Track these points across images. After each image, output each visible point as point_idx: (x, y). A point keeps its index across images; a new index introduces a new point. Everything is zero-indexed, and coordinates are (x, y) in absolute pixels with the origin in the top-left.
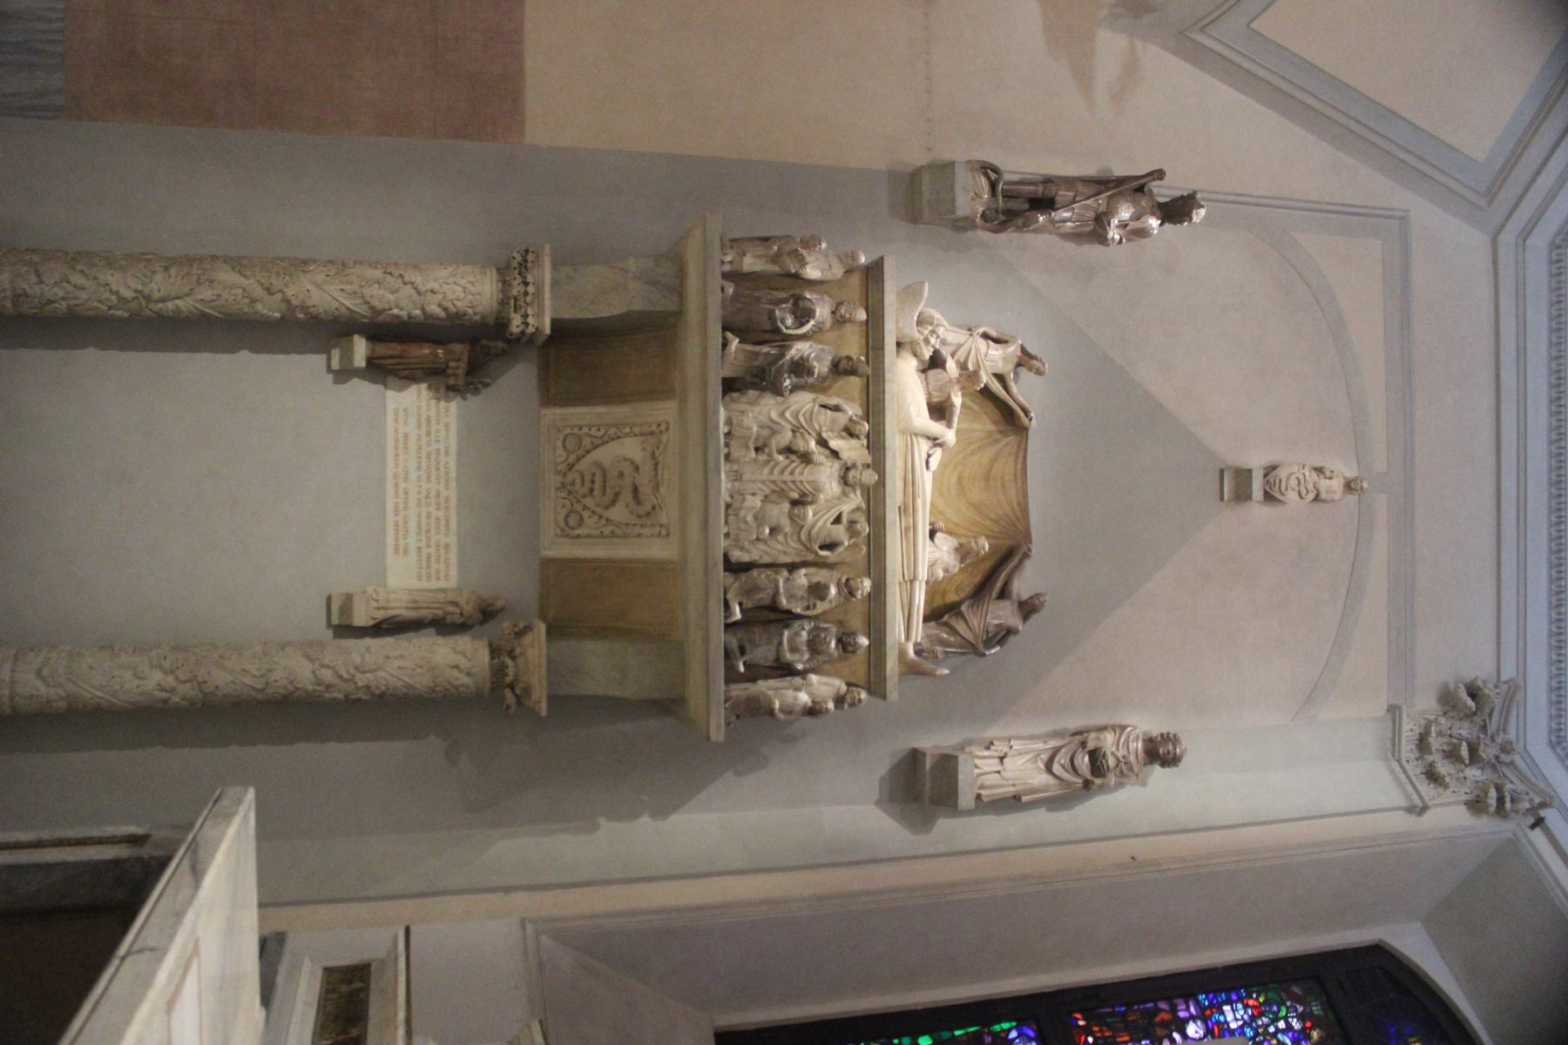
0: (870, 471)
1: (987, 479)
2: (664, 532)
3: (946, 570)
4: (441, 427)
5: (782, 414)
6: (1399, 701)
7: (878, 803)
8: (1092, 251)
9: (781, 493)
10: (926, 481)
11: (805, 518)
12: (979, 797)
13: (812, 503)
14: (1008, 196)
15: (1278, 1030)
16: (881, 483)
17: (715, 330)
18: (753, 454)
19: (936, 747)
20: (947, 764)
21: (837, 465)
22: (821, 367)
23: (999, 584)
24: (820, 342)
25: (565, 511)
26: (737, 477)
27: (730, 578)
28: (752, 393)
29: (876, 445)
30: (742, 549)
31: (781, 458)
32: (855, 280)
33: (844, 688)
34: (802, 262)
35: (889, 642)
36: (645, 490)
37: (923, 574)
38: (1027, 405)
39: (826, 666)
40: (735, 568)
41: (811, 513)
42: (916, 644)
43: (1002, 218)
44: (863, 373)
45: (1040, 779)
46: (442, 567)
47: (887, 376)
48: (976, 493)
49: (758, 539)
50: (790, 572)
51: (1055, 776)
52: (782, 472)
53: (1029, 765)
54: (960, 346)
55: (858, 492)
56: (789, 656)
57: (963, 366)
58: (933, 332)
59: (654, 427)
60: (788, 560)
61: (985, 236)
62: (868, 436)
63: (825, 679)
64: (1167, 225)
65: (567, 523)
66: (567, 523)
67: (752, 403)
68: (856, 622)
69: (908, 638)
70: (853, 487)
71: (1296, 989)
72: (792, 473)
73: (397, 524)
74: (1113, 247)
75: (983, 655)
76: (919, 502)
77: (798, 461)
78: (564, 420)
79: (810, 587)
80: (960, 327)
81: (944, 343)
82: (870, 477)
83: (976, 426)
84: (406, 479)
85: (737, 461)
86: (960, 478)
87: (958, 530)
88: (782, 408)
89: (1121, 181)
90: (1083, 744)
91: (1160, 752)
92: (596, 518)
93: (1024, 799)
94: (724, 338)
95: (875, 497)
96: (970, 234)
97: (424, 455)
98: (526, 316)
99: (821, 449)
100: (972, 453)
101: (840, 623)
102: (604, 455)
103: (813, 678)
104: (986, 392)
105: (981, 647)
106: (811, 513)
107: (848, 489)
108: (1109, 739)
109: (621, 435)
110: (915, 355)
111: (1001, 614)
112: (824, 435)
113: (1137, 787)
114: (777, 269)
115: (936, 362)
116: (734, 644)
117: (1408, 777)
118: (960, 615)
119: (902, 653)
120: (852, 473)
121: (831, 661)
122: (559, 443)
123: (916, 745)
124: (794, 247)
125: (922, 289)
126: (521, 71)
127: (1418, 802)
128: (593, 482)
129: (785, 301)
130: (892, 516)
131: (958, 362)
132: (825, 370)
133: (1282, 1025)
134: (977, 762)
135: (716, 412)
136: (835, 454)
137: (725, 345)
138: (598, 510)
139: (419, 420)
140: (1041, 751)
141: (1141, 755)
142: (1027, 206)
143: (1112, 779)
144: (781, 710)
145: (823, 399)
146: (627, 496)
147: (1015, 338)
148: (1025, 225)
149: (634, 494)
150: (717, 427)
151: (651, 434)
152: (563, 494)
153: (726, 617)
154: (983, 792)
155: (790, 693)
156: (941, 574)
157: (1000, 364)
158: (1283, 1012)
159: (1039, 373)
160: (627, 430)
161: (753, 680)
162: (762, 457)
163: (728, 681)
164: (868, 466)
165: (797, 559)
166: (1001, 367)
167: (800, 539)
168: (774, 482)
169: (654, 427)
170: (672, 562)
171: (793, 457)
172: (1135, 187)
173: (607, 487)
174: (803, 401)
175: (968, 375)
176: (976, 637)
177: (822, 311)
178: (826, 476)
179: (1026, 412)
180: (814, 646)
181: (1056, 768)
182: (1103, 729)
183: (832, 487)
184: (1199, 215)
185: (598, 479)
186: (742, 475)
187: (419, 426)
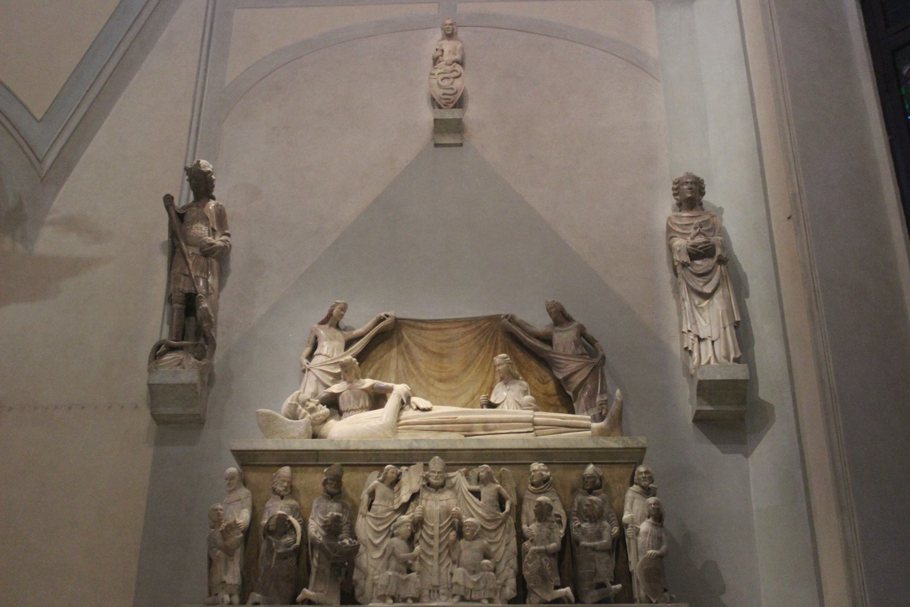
0: (431, 463)
3: (525, 393)
5: (377, 547)
7: (747, 455)
8: (236, 260)
9: (451, 548)
10: (441, 411)
11: (472, 525)
12: (737, 360)
13: (460, 519)
16: (442, 453)
18: (413, 575)
19: (691, 400)
20: (706, 389)
21: (425, 495)
22: (334, 509)
23: (539, 344)
27: (532, 598)
28: (356, 575)
29: (407, 457)
30: (504, 586)
31: (417, 548)
32: (254, 476)
34: (233, 526)
35: (590, 444)
37: (528, 414)
38: (374, 319)
39: (615, 504)
40: (522, 592)
41: (469, 520)
42: (594, 419)
43: (202, 341)
45: (717, 304)
47: (343, 447)
48: (454, 366)
49: (494, 571)
50: (525, 539)
52: (431, 547)
53: (706, 314)
54: (318, 380)
55: (451, 474)
56: (606, 541)
57: (337, 378)
58: (304, 405)
60: (514, 541)
61: (219, 355)
63: (627, 506)
64: (215, 193)
67: (365, 574)
68: (572, 476)
69: (588, 428)
70: (446, 479)
72: (432, 537)
76: (461, 417)
77: (420, 532)
79: (539, 521)
81: (315, 395)
82: (436, 464)
83: (393, 365)
85: (420, 591)
86: (441, 380)
87: (489, 380)
88: (370, 547)
89: (173, 234)
90: (684, 265)
91: (691, 195)
95: (455, 459)
96: (215, 370)
99: (410, 510)
100: (417, 368)
101: (574, 491)
103: (626, 516)
104: (361, 357)
105: (596, 360)
106: (469, 520)
107: (448, 484)
108: (678, 242)
110: (325, 421)
111: (564, 338)
112: (397, 506)
114: (239, 552)
116: (595, 593)
119: (603, 433)
120: (433, 481)
124: (218, 535)
125: (262, 414)
129: (270, 543)
130: (472, 443)
131: (334, 382)
132: (335, 506)
136: (415, 496)
137: (310, 602)
142: (192, 318)
143: (716, 239)
144: (658, 548)
148: (209, 319)
153: (570, 602)
154: (732, 356)
155: (640, 539)
156: (528, 398)
157: (336, 343)
159: (344, 309)
161: (630, 574)
162: (417, 566)
163: (631, 600)
164: (426, 465)
168: (440, 555)
171: (417, 536)
172: (179, 220)
174: (365, 526)
175: (345, 372)
176: (587, 364)
177: (279, 508)
178: (434, 505)
179: (381, 320)
180: (595, 517)
181: (708, 289)
182: (670, 249)
184: (206, 165)
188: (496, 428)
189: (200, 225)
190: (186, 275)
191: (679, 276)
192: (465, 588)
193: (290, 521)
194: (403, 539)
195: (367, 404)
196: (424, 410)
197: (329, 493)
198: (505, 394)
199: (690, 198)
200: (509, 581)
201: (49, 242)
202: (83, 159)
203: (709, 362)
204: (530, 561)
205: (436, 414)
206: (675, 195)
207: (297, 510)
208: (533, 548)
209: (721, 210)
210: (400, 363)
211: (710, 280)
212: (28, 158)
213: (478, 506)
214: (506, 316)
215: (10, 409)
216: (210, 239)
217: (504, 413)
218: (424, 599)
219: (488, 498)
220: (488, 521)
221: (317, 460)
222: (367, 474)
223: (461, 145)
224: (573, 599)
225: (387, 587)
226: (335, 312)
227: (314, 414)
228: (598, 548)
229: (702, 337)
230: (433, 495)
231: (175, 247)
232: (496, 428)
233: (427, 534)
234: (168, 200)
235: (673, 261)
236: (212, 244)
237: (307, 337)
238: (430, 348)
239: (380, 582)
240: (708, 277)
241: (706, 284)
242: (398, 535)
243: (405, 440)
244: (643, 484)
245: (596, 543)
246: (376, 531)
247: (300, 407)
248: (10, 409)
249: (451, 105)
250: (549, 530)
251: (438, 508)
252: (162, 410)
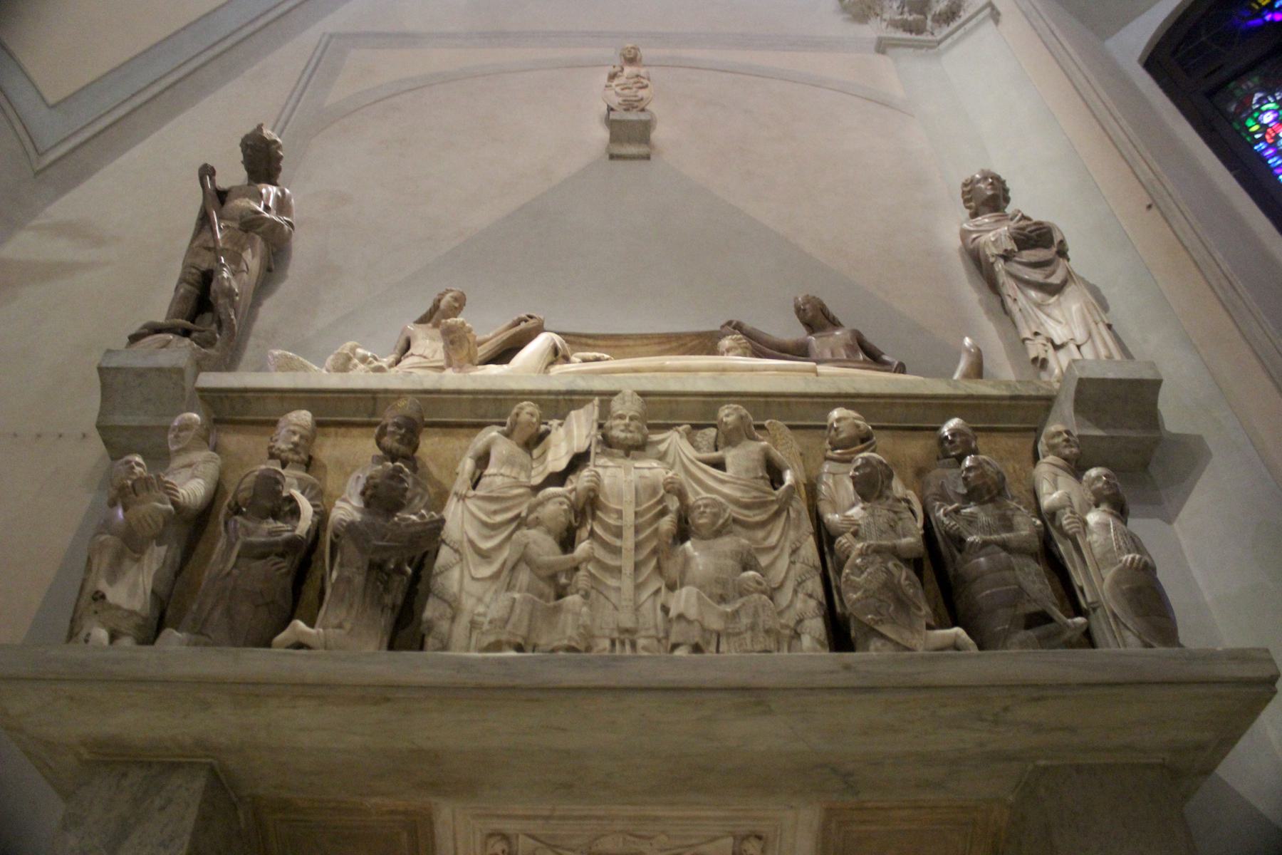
5: (485, 556)
7: (1169, 521)
13: (681, 495)
31: (583, 548)
38: (509, 322)
52: (616, 551)
60: (809, 549)
71: (1232, 108)
120: (618, 433)
135: (464, 665)
136: (578, 461)
145: (461, 484)
165: (807, 526)
167: (762, 525)
168: (637, 566)
170: (825, 828)
178: (617, 478)
180: (986, 490)
183: (650, 469)
190: (209, 249)
192: (704, 630)
193: (291, 499)
194: (549, 532)
200: (807, 623)
204: (860, 569)
206: (966, 201)
212: (21, 141)
213: (722, 482)
220: (747, 506)
221: (373, 414)
225: (506, 621)
226: (443, 304)
228: (1014, 544)
229: (1058, 342)
230: (620, 461)
233: (606, 527)
234: (207, 172)
237: (396, 340)
242: (537, 523)
244: (1067, 451)
245: (1005, 535)
246: (485, 524)
250: (892, 515)
252: (118, 419)
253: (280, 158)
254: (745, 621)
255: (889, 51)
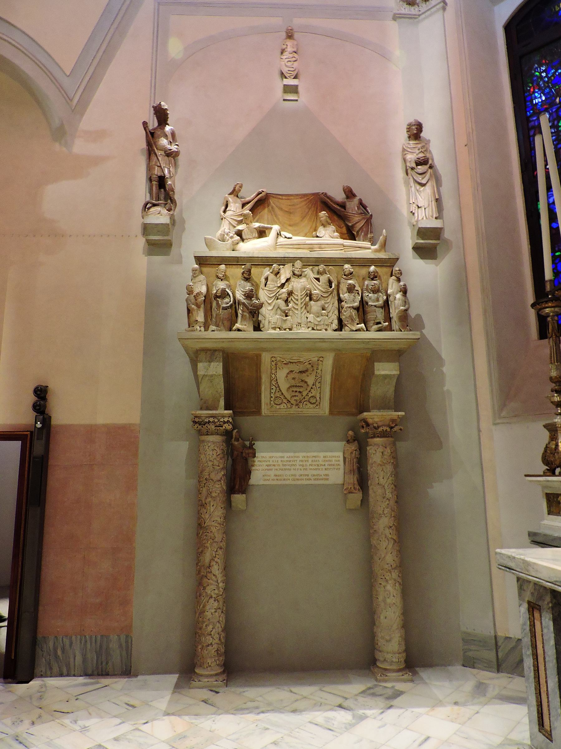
0: (295, 264)
1: (290, 213)
2: (321, 359)
4: (271, 460)
6: (391, 15)
8: (181, 159)
9: (306, 305)
10: (297, 239)
12: (436, 218)
13: (310, 291)
14: (158, 199)
15: (547, 76)
16: (300, 259)
17: (233, 334)
19: (412, 238)
20: (423, 233)
21: (292, 279)
22: (248, 286)
24: (236, 287)
25: (309, 405)
26: (299, 324)
28: (260, 318)
29: (283, 261)
30: (332, 323)
33: (393, 277)
34: (199, 294)
35: (372, 256)
36: (302, 368)
44: (249, 265)
45: (428, 190)
46: (334, 459)
48: (296, 218)
51: (427, 182)
52: (297, 304)
53: (422, 194)
55: (304, 270)
56: (381, 302)
57: (240, 222)
58: (227, 234)
59: (273, 363)
60: (336, 302)
62: (279, 265)
63: (390, 286)
64: (168, 122)
65: (314, 403)
66: (314, 403)
68: (363, 271)
72: (297, 300)
73: (315, 480)
74: (180, 149)
75: (371, 215)
76: (307, 242)
77: (291, 297)
78: (267, 404)
79: (349, 293)
80: (220, 224)
82: (298, 264)
83: (266, 217)
84: (295, 475)
86: (290, 225)
89: (149, 144)
90: (413, 169)
91: (416, 132)
92: (312, 390)
93: (437, 197)
94: (235, 330)
95: (308, 262)
97: (284, 467)
98: (224, 422)
99: (285, 287)
100: (278, 219)
101: (364, 279)
102: (284, 386)
103: (389, 292)
108: (409, 157)
109: (275, 381)
110: (238, 243)
111: (352, 206)
112: (279, 285)
113: (431, 144)
114: (202, 306)
115: (239, 233)
116: (376, 327)
117: (428, 10)
118: (353, 226)
119: (376, 251)
120: (296, 272)
121: (381, 283)
122: (278, 407)
123: (411, 248)
126: (105, 426)
127: (442, 4)
128: (296, 391)
129: (218, 303)
130: (315, 255)
131: (238, 225)
132: (249, 284)
133: (544, 74)
134: (420, 218)
135: (271, 334)
136: (288, 280)
137: (239, 330)
138: (309, 390)
139: (268, 470)
140: (415, 187)
141: (417, 142)
142: (162, 190)
143: (428, 155)
146: (304, 376)
147: (225, 197)
149: (303, 373)
150: (277, 333)
151: (276, 365)
152: (301, 405)
154: (434, 216)
155: (396, 302)
156: (336, 234)
157: (237, 205)
158: (537, 74)
159: (241, 187)
160: (273, 376)
162: (290, 313)
165: (336, 298)
166: (239, 205)
169: (273, 363)
170: (335, 356)
171: (289, 299)
172: (151, 137)
173: (299, 386)
174: (263, 295)
176: (364, 218)
177: (221, 285)
178: (297, 285)
180: (376, 291)
181: (424, 181)
182: (405, 160)
183: (303, 280)
184: (164, 105)
185: (295, 389)
186: (297, 323)
187: (271, 470)
188: (325, 248)
189: (162, 138)
191: (409, 174)
195: (257, 235)
196: (289, 238)
197: (244, 277)
198: (324, 232)
199: (416, 133)
201: (80, 147)
202: (95, 97)
203: (423, 219)
204: (345, 311)
205: (295, 240)
206: (407, 131)
207: (230, 286)
208: (346, 305)
209: (429, 141)
210: (269, 217)
211: (425, 177)
214: (323, 193)
215: (70, 236)
216: (169, 147)
217: (324, 240)
218: (293, 329)
219: (324, 281)
222: (263, 269)
223: (297, 100)
224: (365, 330)
226: (236, 188)
227: (233, 240)
231: (151, 149)
232: (325, 248)
233: (295, 298)
235: (406, 167)
236: (171, 150)
238: (284, 208)
239: (272, 321)
240: (424, 175)
241: (423, 178)
242: (280, 298)
243: (280, 253)
244: (397, 276)
247: (226, 236)
248: (70, 236)
249: (293, 77)
251: (300, 286)
253: (168, 114)
254: (322, 323)
255: (398, 20)
